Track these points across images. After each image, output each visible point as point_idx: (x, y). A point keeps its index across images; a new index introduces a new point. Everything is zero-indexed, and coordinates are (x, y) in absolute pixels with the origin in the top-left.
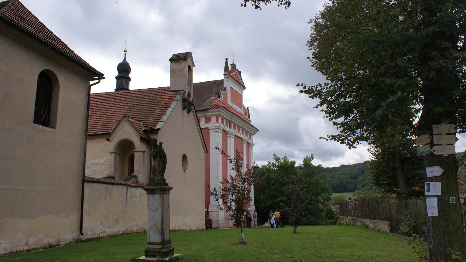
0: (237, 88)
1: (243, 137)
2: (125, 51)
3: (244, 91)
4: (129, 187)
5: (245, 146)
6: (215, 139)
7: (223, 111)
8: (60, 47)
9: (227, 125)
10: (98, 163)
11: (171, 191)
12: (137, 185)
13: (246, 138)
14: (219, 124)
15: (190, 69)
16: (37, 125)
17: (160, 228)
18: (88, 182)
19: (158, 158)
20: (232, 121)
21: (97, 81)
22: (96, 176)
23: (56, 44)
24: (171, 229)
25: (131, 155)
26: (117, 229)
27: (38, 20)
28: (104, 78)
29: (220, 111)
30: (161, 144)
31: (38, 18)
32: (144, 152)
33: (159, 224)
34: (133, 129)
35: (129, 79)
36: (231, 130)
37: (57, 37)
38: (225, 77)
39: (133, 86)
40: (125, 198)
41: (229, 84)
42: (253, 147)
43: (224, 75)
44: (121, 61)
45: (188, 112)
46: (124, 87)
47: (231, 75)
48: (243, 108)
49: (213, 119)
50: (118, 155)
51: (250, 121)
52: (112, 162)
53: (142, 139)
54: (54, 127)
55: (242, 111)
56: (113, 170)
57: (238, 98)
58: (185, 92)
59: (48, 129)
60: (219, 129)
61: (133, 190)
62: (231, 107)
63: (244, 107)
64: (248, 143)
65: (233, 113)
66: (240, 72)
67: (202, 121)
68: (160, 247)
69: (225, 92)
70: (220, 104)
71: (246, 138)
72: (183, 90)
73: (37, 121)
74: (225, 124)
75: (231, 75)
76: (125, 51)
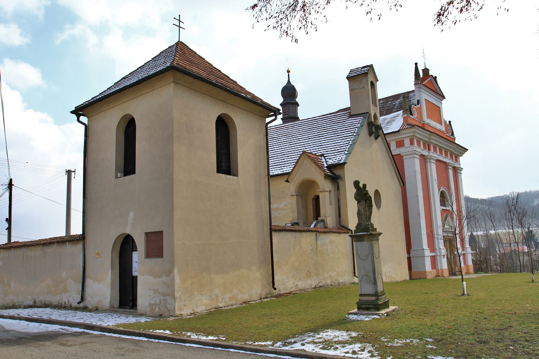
0: (433, 100)
1: (447, 160)
2: (288, 72)
3: (444, 101)
4: (318, 233)
5: (451, 172)
6: (413, 167)
7: (419, 132)
8: (231, 86)
9: (425, 148)
10: (277, 208)
11: (380, 237)
12: (326, 230)
13: (451, 162)
14: (415, 147)
15: (373, 85)
16: (220, 175)
17: (372, 279)
18: (276, 231)
19: (363, 202)
20: (431, 142)
21: (274, 117)
22: (282, 224)
23: (227, 84)
24: (408, 278)
25: (315, 196)
26: (309, 282)
27: (204, 59)
28: (72, 112)
29: (415, 132)
30: (365, 186)
31: (204, 57)
32: (330, 191)
33: (371, 275)
34: (313, 165)
35: (297, 104)
36: (431, 154)
37: (226, 75)
38: (416, 88)
39: (303, 113)
40: (315, 247)
41: (425, 96)
42: (462, 172)
43: (415, 84)
44: (285, 83)
45: (376, 138)
46: (292, 115)
47: (424, 83)
48: (443, 123)
49: (407, 142)
50: (300, 198)
51: (454, 139)
52: (295, 206)
53: (326, 177)
54: (236, 175)
55: (443, 128)
56: (295, 215)
57: (436, 112)
58: (370, 115)
59: (231, 177)
60: (415, 154)
61: (322, 236)
62: (428, 125)
63: (445, 122)
64: (454, 168)
65: (431, 132)
66: (436, 77)
67: (393, 146)
68: (373, 298)
69: (419, 106)
70: (414, 123)
71: (451, 162)
72: (367, 113)
73: (220, 170)
74: (422, 148)
75: (424, 83)
76: (288, 72)
